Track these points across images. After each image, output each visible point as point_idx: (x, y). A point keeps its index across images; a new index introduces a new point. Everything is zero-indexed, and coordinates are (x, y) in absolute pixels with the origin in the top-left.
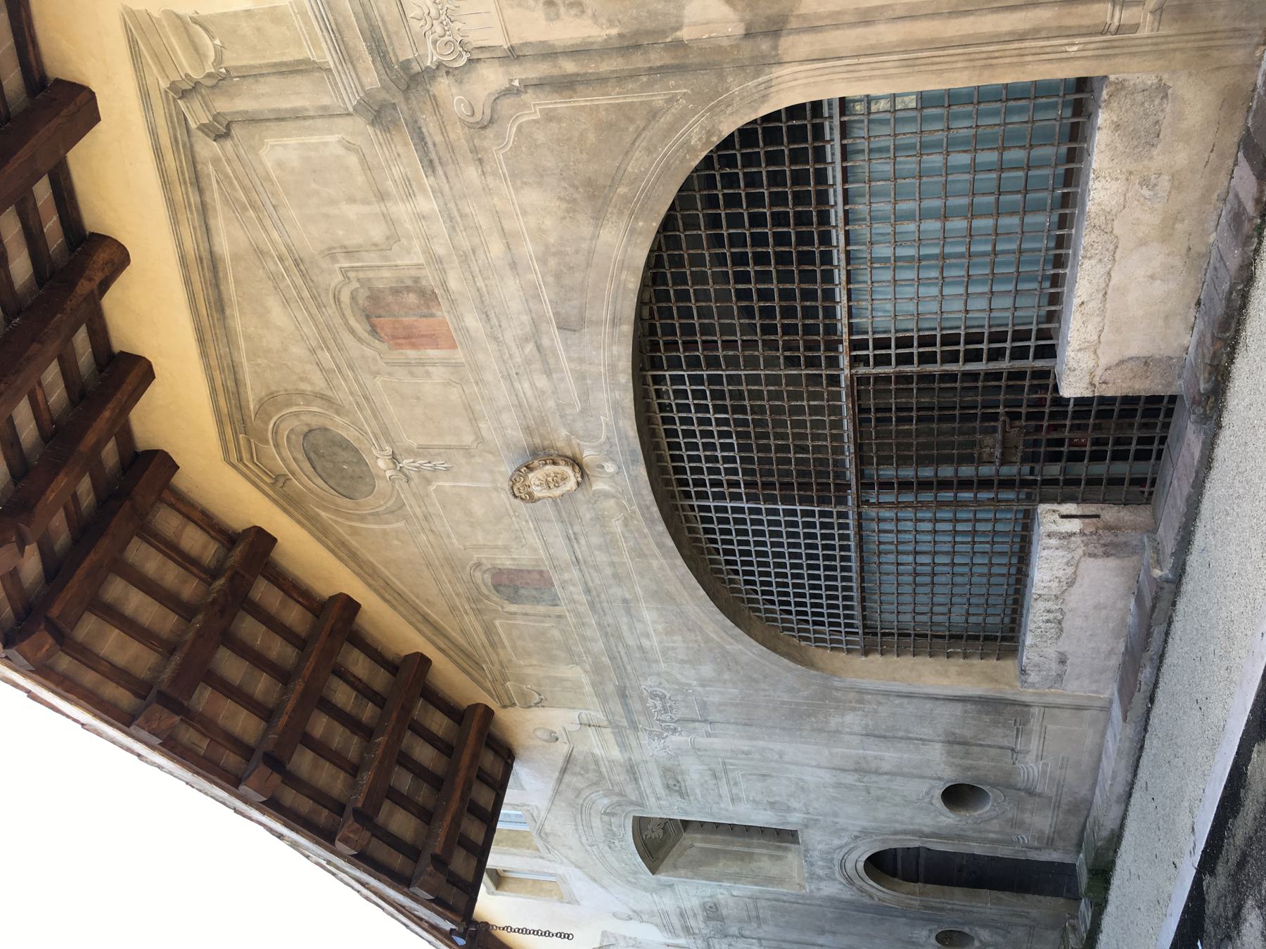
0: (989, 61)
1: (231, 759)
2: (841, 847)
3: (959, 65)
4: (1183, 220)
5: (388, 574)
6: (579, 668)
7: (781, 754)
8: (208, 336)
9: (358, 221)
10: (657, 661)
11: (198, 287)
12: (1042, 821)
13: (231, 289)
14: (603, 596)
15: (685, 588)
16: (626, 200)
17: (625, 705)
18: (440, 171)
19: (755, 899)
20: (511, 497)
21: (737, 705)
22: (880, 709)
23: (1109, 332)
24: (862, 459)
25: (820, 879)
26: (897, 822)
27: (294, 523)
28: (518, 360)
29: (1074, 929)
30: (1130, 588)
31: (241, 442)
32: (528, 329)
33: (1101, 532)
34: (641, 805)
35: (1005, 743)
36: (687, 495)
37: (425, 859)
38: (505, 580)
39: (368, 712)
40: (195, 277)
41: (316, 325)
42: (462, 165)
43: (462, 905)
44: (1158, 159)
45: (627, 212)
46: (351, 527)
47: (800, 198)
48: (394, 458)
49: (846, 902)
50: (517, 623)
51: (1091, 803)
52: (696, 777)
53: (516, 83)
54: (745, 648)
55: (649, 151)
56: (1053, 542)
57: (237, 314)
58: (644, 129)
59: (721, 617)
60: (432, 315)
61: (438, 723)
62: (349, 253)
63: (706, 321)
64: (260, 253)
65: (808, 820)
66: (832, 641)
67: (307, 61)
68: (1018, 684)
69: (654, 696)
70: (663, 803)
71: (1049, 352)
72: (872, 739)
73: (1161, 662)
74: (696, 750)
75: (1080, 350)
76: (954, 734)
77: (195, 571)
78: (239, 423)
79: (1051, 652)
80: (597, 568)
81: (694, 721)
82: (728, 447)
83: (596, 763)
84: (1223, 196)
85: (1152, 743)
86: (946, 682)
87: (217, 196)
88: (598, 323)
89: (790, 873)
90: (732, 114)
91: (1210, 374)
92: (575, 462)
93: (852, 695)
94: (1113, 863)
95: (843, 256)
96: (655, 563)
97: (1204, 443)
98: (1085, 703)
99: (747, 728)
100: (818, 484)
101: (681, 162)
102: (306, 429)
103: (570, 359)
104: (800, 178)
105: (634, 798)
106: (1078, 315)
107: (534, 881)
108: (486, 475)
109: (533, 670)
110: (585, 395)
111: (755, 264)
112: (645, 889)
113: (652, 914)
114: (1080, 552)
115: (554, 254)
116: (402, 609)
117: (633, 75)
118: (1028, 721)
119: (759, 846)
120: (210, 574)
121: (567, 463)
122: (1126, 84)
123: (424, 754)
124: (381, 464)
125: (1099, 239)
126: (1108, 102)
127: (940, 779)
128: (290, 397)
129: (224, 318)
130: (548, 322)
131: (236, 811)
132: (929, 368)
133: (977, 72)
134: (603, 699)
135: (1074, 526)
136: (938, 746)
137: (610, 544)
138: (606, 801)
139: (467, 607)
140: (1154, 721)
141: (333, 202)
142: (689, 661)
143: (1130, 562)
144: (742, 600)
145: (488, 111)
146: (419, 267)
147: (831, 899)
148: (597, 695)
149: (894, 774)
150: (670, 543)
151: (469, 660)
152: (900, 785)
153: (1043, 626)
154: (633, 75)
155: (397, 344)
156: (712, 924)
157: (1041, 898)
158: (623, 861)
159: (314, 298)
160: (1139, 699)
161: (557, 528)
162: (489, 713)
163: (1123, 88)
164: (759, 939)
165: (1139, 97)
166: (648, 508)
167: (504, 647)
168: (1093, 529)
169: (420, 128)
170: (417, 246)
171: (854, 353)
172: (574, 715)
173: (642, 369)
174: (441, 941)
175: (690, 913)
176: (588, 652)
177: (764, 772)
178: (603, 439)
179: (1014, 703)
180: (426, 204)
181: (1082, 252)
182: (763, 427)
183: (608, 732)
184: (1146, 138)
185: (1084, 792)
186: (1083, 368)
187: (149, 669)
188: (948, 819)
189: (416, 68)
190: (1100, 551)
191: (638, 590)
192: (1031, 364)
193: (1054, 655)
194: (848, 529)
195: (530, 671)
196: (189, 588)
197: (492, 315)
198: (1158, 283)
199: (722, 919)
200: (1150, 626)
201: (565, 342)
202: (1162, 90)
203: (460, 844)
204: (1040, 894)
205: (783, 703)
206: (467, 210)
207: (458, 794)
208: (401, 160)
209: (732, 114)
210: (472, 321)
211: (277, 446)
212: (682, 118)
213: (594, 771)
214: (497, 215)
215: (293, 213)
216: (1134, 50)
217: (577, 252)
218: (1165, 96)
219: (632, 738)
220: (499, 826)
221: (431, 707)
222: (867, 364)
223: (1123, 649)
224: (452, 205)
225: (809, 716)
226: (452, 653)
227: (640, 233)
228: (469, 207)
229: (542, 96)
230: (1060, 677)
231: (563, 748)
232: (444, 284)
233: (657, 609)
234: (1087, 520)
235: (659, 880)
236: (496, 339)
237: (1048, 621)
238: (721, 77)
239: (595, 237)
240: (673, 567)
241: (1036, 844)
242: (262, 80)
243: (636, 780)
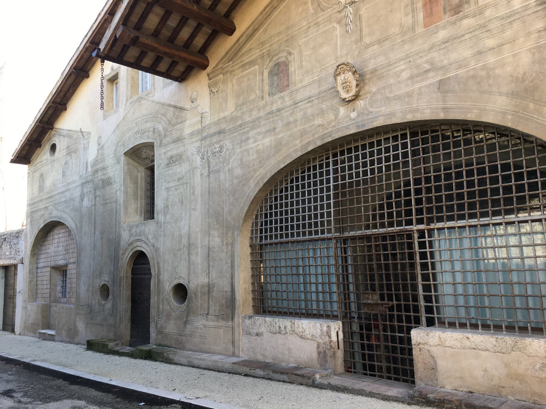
2: (148, 239)
4: (521, 384)
5: (281, 7)
6: (233, 109)
7: (194, 209)
10: (241, 147)
12: (171, 328)
14: (276, 118)
15: (285, 157)
17: (215, 134)
18: (539, 8)
19: (116, 202)
20: (337, 64)
22: (224, 254)
23: (447, 352)
26: (164, 264)
28: (419, 61)
29: (117, 345)
30: (301, 364)
34: (160, 146)
36: (335, 155)
37: (136, 33)
43: (112, 54)
45: (517, 109)
50: (257, 77)
51: (183, 350)
52: (179, 170)
54: (252, 189)
56: (325, 329)
59: (269, 176)
60: (445, 13)
61: (199, 41)
63: (442, 157)
65: (161, 224)
66: (257, 230)
68: (243, 315)
69: (221, 147)
70: (163, 156)
71: (430, 323)
72: (207, 250)
73: (268, 379)
74: (193, 170)
75: (440, 338)
76: (214, 287)
79: (263, 329)
80: (292, 114)
81: (209, 167)
82: (351, 176)
83: (181, 122)
84: (536, 402)
85: (225, 377)
86: (241, 282)
89: (130, 216)
92: (357, 97)
94: (156, 361)
97: (397, 397)
99: (207, 193)
103: (420, 89)
105: (164, 142)
107: (113, 98)
108: (345, 52)
109: (230, 87)
110: (398, 98)
111: (479, 180)
112: (115, 151)
113: (103, 154)
114: (320, 341)
116: (260, 18)
119: (141, 203)
121: (357, 92)
123: (185, 33)
130: (444, 74)
135: (334, 338)
136: (206, 280)
137: (307, 119)
138: (161, 128)
139: (264, 51)
140: (237, 377)
142: (242, 163)
143: (316, 363)
144: (276, 186)
147: (120, 236)
148: (219, 120)
149: (189, 262)
150: (310, 148)
151: (234, 54)
156: (101, 183)
158: (130, 139)
160: (246, 370)
162: (204, 67)
164: (95, 205)
166: (330, 136)
168: (333, 346)
171: (426, 231)
172: (207, 110)
174: (79, 54)
175: (105, 172)
176: (243, 113)
177: (184, 202)
178: (371, 110)
182: (378, 190)
185: (188, 346)
186: (425, 340)
188: (168, 287)
190: (321, 349)
191: (282, 135)
193: (261, 331)
194: (291, 237)
195: (230, 86)
197: (447, 45)
198: (482, 373)
199: (103, 187)
200: (287, 374)
205: (223, 209)
206: (514, 25)
207: (168, 50)
210: (442, 34)
214: (512, 41)
217: (489, 85)
219: (197, 138)
221: (207, 37)
224: (518, 16)
225: (216, 221)
226: (237, 45)
228: (516, 26)
231: (188, 105)
232: (466, 17)
233: (271, 145)
234: (337, 343)
235: (121, 156)
236: (432, 48)
237: (280, 327)
239: (500, 94)
240: (296, 151)
241: (159, 326)
243: (174, 142)
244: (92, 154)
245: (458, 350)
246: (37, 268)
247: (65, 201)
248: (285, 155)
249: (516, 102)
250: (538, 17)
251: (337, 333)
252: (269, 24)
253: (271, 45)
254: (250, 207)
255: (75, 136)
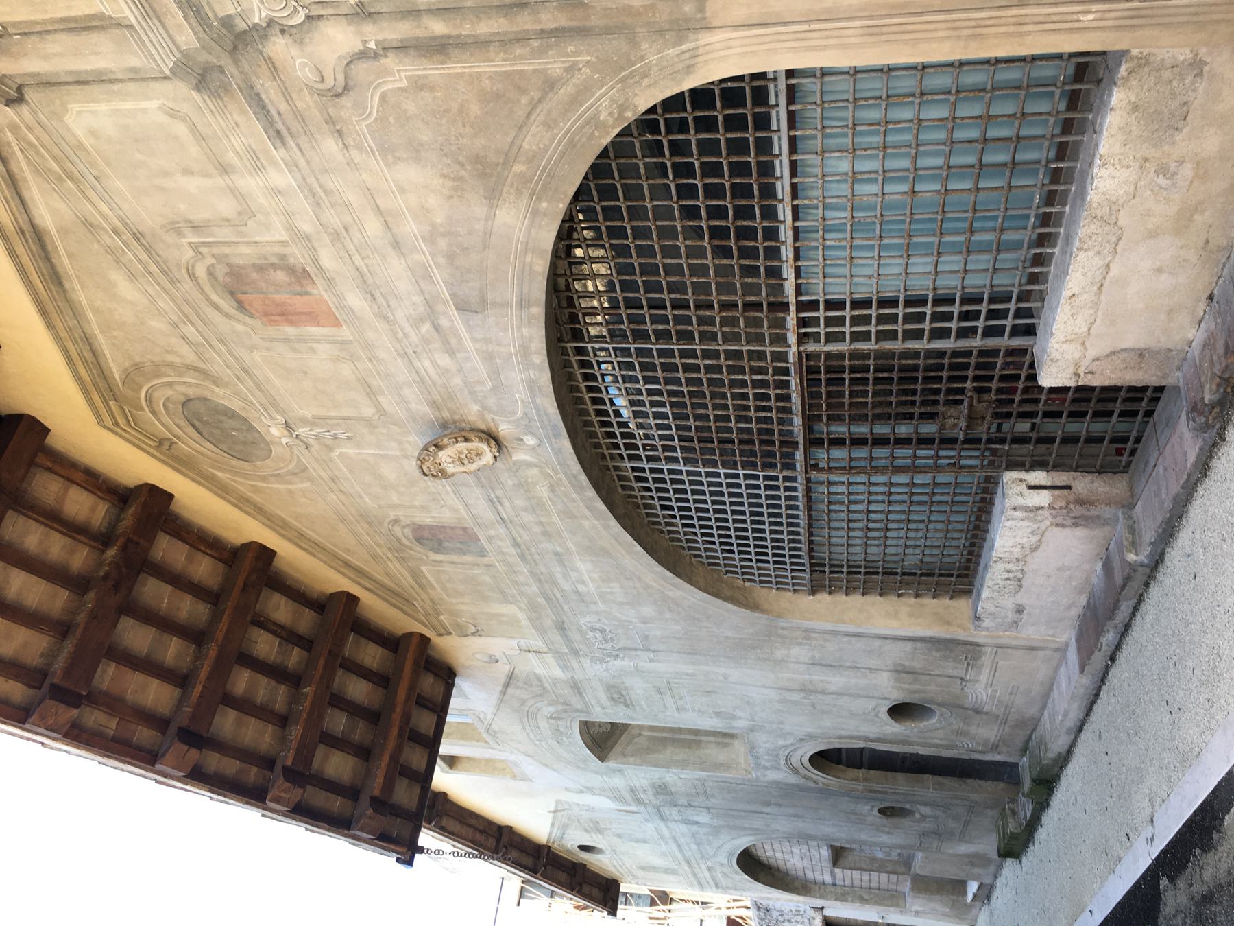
0: (978, 31)
1: (144, 735)
2: (787, 746)
3: (940, 34)
4: (1203, 212)
8: (50, 308)
9: (200, 195)
11: (25, 259)
13: (64, 261)
14: (533, 550)
16: (524, 179)
18: (291, 142)
21: (679, 639)
24: (810, 420)
25: (766, 768)
27: (188, 481)
29: (1014, 812)
31: (114, 408)
32: (422, 309)
33: (1072, 506)
34: (587, 712)
35: (955, 673)
37: (365, 800)
38: (426, 534)
39: (294, 658)
40: (20, 249)
41: (173, 300)
42: (318, 136)
44: (1183, 145)
45: (526, 193)
46: (252, 486)
47: (740, 169)
48: (287, 426)
49: (792, 785)
50: (443, 574)
51: (1039, 720)
52: (640, 692)
53: (372, 45)
55: (549, 125)
57: (78, 287)
58: (540, 101)
59: (660, 569)
60: (307, 293)
61: (372, 655)
62: (196, 228)
64: (89, 225)
67: (101, 17)
68: (971, 627)
69: (593, 629)
71: (1030, 331)
74: (638, 671)
77: (83, 539)
78: (106, 391)
79: (1009, 603)
80: (523, 526)
81: (636, 649)
86: (895, 624)
87: (24, 165)
88: (504, 305)
90: (649, 86)
91: (1218, 386)
92: (491, 437)
93: (798, 633)
95: (790, 233)
96: (586, 524)
98: (1042, 644)
100: (765, 449)
101: (589, 139)
102: (183, 399)
103: (474, 340)
104: (739, 147)
105: (579, 707)
106: (1067, 308)
108: (394, 445)
109: (467, 607)
110: (495, 373)
114: (1048, 523)
115: (443, 235)
117: (521, 39)
118: (980, 657)
120: (103, 539)
122: (1152, 59)
123: (358, 690)
124: (275, 431)
125: (1100, 231)
126: (1127, 79)
127: (886, 698)
128: (157, 370)
129: (65, 291)
130: (445, 303)
131: (157, 782)
132: (888, 345)
133: (962, 43)
134: (542, 631)
135: (1043, 498)
136: (886, 675)
138: (551, 709)
139: (390, 555)
141: (166, 174)
143: (1099, 533)
145: (340, 77)
146: (283, 243)
147: (776, 783)
150: (602, 507)
152: (844, 701)
153: (1002, 583)
154: (521, 39)
155: (271, 321)
156: (661, 797)
157: (981, 782)
159: (164, 272)
160: (1099, 659)
161: (478, 492)
162: (424, 641)
163: (1147, 63)
165: (1167, 75)
167: (433, 588)
169: (258, 95)
170: (277, 223)
171: (803, 330)
172: (514, 643)
173: (560, 340)
176: (521, 594)
178: (519, 414)
179: (965, 643)
180: (281, 178)
181: (1077, 244)
183: (549, 658)
184: (1166, 121)
185: (1032, 712)
186: (1068, 350)
187: (42, 655)
188: (894, 728)
189: (242, 26)
190: (1069, 522)
192: (1005, 342)
196: (79, 558)
198: (1164, 276)
200: (1118, 601)
201: (466, 323)
202: (1197, 67)
203: (402, 774)
204: (981, 778)
205: (727, 638)
208: (240, 131)
209: (649, 86)
210: (355, 300)
211: (153, 412)
212: (586, 90)
213: (539, 687)
214: (370, 193)
215: (120, 185)
216: (1167, 20)
218: (1200, 74)
220: (448, 719)
221: (363, 640)
222: (817, 340)
223: (1084, 603)
224: (311, 180)
227: (545, 215)
229: (407, 60)
230: (1015, 623)
232: (316, 262)
233: (592, 561)
234: (1057, 492)
236: (386, 318)
238: (634, 43)
240: (606, 527)
242: (48, 37)
243: (580, 694)
244: (604, 804)
245: (1099, 313)
246: (834, 885)
247: (698, 845)
248: (613, 542)
249: (509, 193)
250: (313, 148)
251: (1031, 487)
252: (335, 545)
253: (379, 545)
254: (726, 599)
255: (565, 820)
